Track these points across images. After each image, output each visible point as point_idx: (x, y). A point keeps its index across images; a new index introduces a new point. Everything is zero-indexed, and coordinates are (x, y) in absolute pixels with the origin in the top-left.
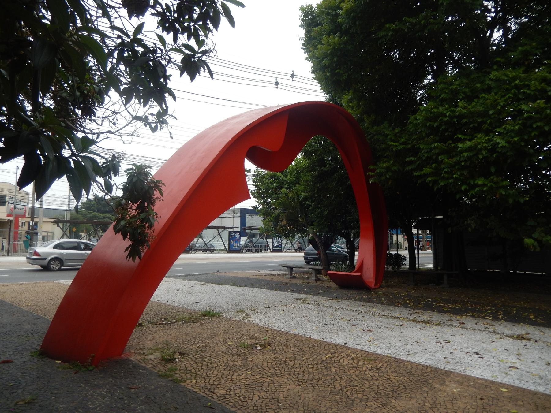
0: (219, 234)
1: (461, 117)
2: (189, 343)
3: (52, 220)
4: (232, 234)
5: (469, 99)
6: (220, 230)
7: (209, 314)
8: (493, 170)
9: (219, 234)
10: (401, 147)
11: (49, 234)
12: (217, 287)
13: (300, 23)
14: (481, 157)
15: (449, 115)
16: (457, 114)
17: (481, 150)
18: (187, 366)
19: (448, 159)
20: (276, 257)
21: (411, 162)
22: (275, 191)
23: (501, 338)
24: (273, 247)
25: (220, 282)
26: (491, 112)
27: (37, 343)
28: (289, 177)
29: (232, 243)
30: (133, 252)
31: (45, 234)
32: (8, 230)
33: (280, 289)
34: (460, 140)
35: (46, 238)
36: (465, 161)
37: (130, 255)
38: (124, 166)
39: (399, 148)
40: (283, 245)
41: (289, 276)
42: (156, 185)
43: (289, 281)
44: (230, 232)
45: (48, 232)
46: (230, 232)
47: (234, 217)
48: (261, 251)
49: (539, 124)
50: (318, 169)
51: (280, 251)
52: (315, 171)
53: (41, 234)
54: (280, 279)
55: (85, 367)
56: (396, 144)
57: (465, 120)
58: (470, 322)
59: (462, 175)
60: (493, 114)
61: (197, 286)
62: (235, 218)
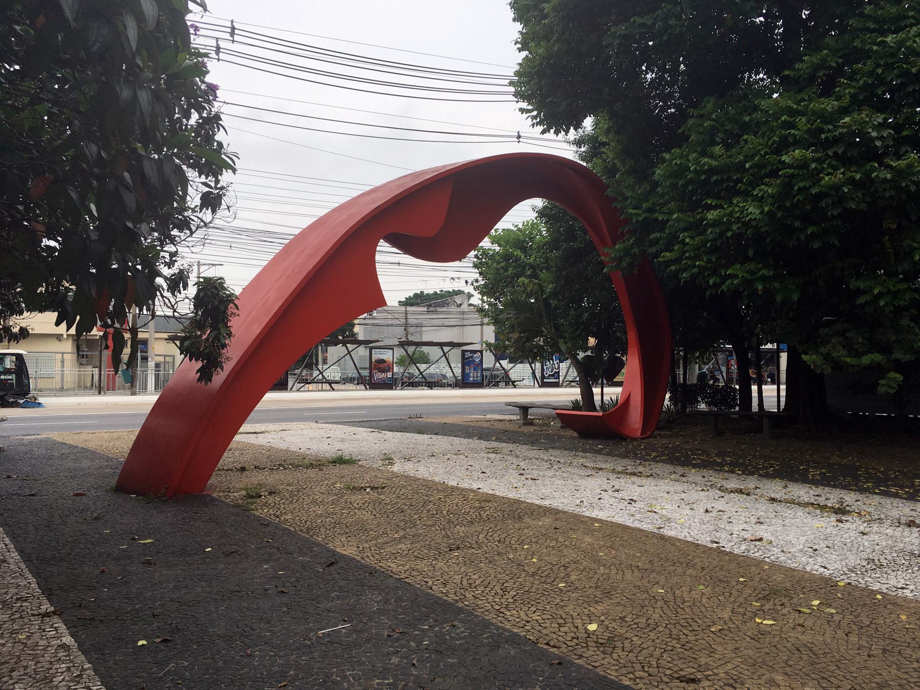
0: (349, 353)
1: (712, 171)
2: (288, 485)
3: (166, 336)
4: (468, 355)
5: (732, 141)
6: (446, 349)
7: (340, 461)
8: (751, 253)
9: (445, 354)
10: (643, 216)
11: (167, 359)
12: (389, 434)
13: (510, 14)
14: (729, 234)
15: (695, 168)
16: (706, 167)
17: (730, 223)
18: (270, 502)
19: (692, 238)
20: (547, 395)
21: (656, 242)
22: (511, 282)
23: (703, 490)
24: (543, 377)
25: (421, 430)
26: (747, 166)
27: (114, 481)
28: (533, 258)
29: (467, 371)
30: (205, 374)
31: (161, 359)
32: (97, 353)
33: (480, 438)
34: (709, 208)
35: (162, 365)
36: (715, 240)
37: (199, 379)
38: (192, 279)
39: (640, 219)
40: (562, 373)
41: (521, 422)
42: (230, 299)
43: (527, 430)
44: (464, 352)
45: (165, 356)
46: (464, 352)
47: (482, 325)
48: (496, 385)
49: (802, 185)
50: (565, 245)
51: (556, 385)
52: (557, 249)
53: (153, 359)
54: (511, 427)
55: (158, 498)
56: (637, 211)
57: (715, 178)
58: (694, 475)
59: (709, 261)
60: (751, 167)
61: (362, 432)
62: (484, 327)
